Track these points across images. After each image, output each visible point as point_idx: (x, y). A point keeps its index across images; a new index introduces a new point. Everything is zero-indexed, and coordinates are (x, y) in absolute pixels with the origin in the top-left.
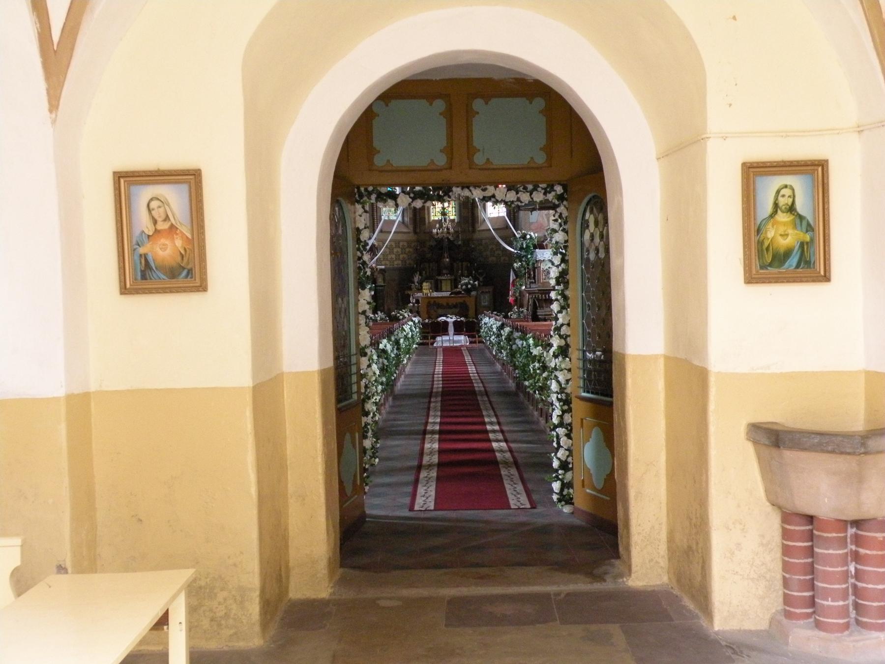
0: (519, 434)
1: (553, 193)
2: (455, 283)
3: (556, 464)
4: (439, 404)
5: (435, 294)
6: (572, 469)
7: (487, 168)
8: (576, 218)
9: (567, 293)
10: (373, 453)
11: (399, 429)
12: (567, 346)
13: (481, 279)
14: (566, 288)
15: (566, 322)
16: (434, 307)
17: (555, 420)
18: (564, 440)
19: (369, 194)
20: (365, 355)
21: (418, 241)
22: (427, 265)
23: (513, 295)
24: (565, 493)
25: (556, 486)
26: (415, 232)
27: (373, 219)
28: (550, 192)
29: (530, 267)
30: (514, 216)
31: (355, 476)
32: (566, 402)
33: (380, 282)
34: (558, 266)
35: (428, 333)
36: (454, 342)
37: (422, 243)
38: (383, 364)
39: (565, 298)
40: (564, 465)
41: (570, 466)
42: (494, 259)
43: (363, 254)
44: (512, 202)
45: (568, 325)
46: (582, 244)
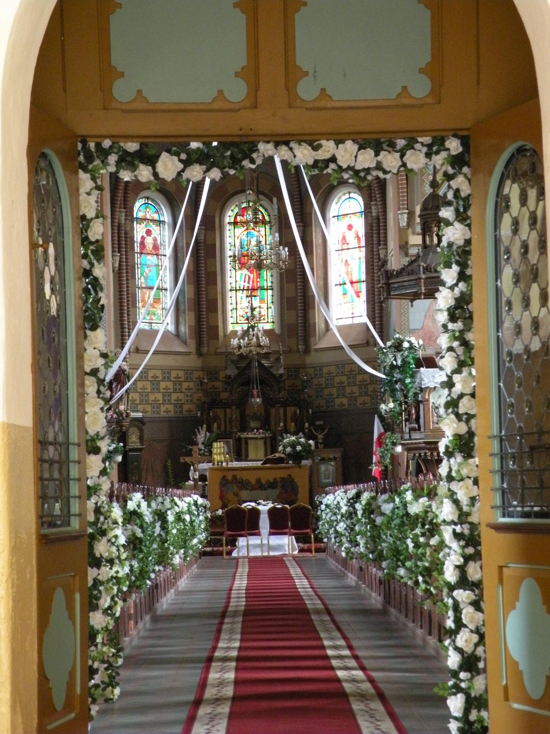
0: (386, 661)
1: (444, 154)
2: (272, 444)
3: (453, 660)
4: (239, 626)
5: (236, 464)
6: (485, 670)
7: (322, 105)
8: (486, 194)
9: (469, 336)
10: (110, 677)
11: (163, 656)
12: (471, 434)
13: (320, 437)
14: (468, 328)
15: (468, 391)
16: (230, 485)
17: (450, 575)
18: (468, 613)
19: (104, 153)
20: (96, 451)
21: (203, 369)
22: (220, 412)
23: (379, 463)
24: (473, 716)
25: (456, 704)
26: (200, 353)
27: (122, 328)
28: (437, 153)
29: (410, 400)
30: (381, 309)
31: (72, 674)
32: (471, 540)
33: (134, 440)
34: (452, 288)
35: (222, 534)
36: (271, 548)
37: (212, 373)
38: (134, 534)
39: (465, 344)
40: (470, 663)
41: (481, 665)
42: (345, 401)
43: (92, 265)
44: (368, 171)
45: (473, 395)
46: (497, 241)
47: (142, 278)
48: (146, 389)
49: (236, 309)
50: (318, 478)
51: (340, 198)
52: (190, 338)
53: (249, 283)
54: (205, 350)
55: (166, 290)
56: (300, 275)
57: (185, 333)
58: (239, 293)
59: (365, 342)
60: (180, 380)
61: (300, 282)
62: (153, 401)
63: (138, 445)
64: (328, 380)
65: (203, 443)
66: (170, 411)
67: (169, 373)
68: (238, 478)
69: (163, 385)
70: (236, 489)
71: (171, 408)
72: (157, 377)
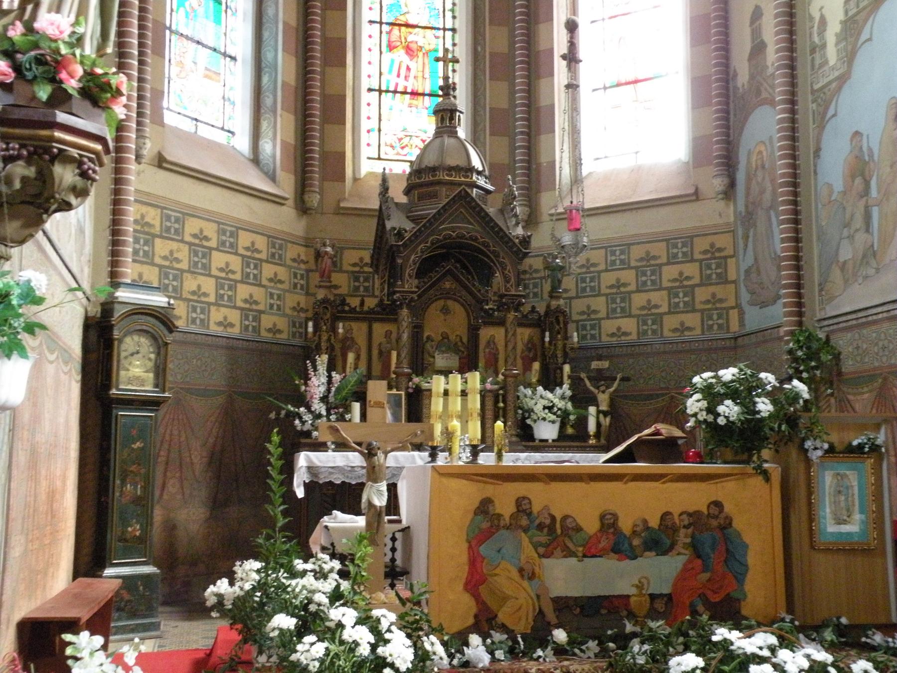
21: (308, 243)
22: (359, 330)
26: (303, 208)
37: (320, 260)
42: (629, 325)
48: (178, 260)
50: (811, 519)
54: (314, 199)
59: (692, 191)
60: (257, 256)
61: (522, 77)
64: (583, 280)
65: (324, 399)
66: (232, 325)
68: (536, 508)
69: (219, 260)
70: (528, 551)
71: (234, 316)
72: (206, 238)
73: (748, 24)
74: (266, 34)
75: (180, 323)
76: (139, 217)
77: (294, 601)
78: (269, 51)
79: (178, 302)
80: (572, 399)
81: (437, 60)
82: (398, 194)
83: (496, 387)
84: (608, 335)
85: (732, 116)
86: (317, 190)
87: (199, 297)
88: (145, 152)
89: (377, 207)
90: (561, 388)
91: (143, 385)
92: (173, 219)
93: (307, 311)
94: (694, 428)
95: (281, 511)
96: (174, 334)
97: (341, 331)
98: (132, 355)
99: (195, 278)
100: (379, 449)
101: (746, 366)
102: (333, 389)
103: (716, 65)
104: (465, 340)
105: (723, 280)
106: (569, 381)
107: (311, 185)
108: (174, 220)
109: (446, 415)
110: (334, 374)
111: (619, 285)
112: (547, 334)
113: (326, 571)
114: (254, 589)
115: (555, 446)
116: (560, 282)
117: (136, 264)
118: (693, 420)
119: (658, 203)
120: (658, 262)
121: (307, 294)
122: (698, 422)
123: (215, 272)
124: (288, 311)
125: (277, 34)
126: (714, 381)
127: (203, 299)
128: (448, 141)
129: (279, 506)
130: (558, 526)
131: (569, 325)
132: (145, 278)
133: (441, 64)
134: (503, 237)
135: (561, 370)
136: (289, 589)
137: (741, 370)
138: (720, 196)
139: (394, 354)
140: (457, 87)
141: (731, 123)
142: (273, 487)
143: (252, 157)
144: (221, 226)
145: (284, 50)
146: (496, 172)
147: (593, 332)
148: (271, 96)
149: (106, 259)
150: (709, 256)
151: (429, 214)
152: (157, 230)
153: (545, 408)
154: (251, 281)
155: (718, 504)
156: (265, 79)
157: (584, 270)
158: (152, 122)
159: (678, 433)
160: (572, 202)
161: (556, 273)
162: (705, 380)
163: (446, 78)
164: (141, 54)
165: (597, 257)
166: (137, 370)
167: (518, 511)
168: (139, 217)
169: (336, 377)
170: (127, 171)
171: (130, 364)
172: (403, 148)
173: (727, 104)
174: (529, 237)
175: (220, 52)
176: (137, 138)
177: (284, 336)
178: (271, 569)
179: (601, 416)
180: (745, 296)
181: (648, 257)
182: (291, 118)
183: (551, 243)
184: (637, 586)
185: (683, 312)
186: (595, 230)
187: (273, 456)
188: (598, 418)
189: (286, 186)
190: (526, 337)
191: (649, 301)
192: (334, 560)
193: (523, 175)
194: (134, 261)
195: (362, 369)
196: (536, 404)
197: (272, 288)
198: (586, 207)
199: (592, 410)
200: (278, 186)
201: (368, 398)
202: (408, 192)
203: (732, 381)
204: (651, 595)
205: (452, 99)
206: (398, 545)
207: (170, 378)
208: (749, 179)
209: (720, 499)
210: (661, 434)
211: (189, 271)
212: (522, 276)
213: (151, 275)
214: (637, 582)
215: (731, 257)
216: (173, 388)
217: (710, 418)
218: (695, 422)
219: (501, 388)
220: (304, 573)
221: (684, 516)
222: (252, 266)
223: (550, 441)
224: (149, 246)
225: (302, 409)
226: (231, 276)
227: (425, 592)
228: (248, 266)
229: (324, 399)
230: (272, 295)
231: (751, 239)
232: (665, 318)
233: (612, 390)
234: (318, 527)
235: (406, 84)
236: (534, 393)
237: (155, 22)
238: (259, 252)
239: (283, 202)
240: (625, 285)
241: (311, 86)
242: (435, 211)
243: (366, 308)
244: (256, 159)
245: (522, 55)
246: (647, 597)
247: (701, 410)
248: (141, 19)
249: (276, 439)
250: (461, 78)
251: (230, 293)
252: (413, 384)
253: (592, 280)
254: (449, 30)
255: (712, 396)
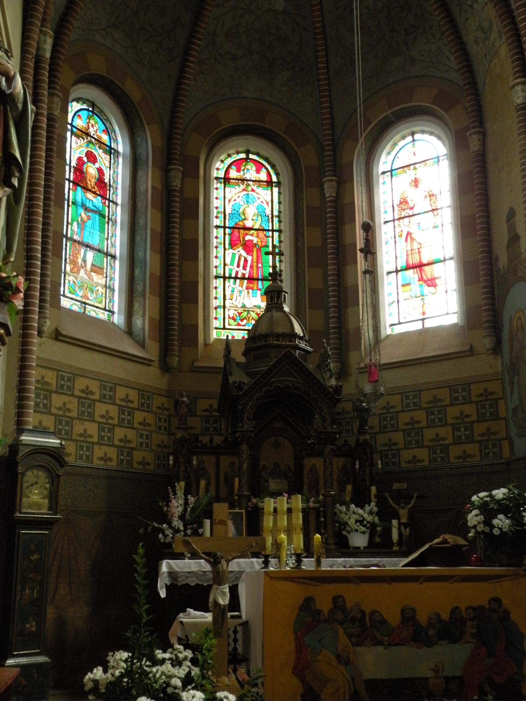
21: (169, 394)
22: (209, 461)
26: (165, 367)
37: (178, 408)
42: (423, 454)
47: (75, 224)
48: (69, 410)
49: (224, 307)
51: (395, 144)
52: (150, 338)
53: (244, 268)
54: (174, 361)
55: (114, 257)
56: (332, 254)
57: (143, 329)
58: (230, 283)
59: (467, 348)
60: (130, 405)
62: (81, 435)
63: (43, 512)
64: (385, 419)
65: (182, 517)
66: (110, 460)
67: (113, 389)
68: (349, 605)
69: (101, 409)
70: (343, 640)
71: (112, 453)
72: (91, 393)
73: (505, 221)
74: (138, 238)
75: (70, 460)
76: (40, 378)
77: (154, 685)
78: (140, 251)
79: (68, 442)
80: (378, 514)
81: (267, 253)
82: (238, 355)
83: (317, 505)
84: (406, 462)
85: (496, 291)
86: (177, 354)
87: (85, 438)
88: (45, 329)
89: (222, 365)
90: (369, 505)
91: (40, 509)
92: (66, 379)
93: (169, 447)
94: (474, 538)
95: (146, 610)
96: (65, 468)
97: (195, 462)
98: (32, 485)
99: (83, 423)
100: (222, 558)
101: (514, 487)
102: (189, 509)
103: (482, 252)
104: (292, 468)
105: (495, 417)
106: (376, 500)
107: (173, 350)
108: (66, 379)
109: (275, 530)
110: (189, 497)
111: (413, 422)
112: (357, 462)
113: (181, 659)
114: (122, 675)
115: (366, 553)
116: (366, 421)
117: (37, 414)
118: (473, 531)
119: (437, 359)
120: (444, 403)
121: (170, 434)
122: (477, 532)
123: (98, 418)
124: (154, 448)
125: (146, 237)
126: (488, 499)
127: (89, 440)
128: (276, 314)
129: (144, 606)
130: (367, 618)
131: (374, 455)
132: (44, 424)
133: (271, 256)
134: (321, 388)
135: (370, 491)
136: (151, 675)
137: (510, 490)
138: (490, 352)
139: (237, 480)
140: (283, 273)
141: (496, 295)
142: (139, 590)
143: (127, 330)
144: (103, 383)
145: (151, 249)
146: (313, 337)
147: (394, 460)
148: (142, 285)
149: (13, 411)
150: (483, 398)
151: (262, 370)
152: (54, 388)
153: (357, 521)
154: (126, 425)
155: (497, 600)
156: (137, 272)
157: (385, 411)
158: (51, 306)
159: (461, 541)
160: (371, 360)
161: (363, 414)
162: (482, 499)
163: (274, 267)
164: (44, 256)
165: (395, 400)
166: (36, 497)
167: (335, 607)
168: (40, 378)
169: (191, 499)
170: (32, 344)
171: (31, 492)
172: (242, 320)
173: (492, 281)
174: (341, 387)
175: (103, 252)
176: (39, 318)
177: (151, 467)
178: (136, 658)
179: (402, 528)
180: (513, 430)
181: (436, 400)
182: (157, 300)
183: (355, 392)
184: (434, 670)
185: (465, 443)
186: (390, 380)
187: (139, 565)
188: (399, 529)
189: (152, 352)
190: (341, 464)
191: (437, 434)
192: (187, 650)
193: (336, 338)
194: (35, 411)
195: (212, 492)
196: (350, 518)
197: (142, 430)
198: (382, 362)
199: (395, 522)
200: (147, 352)
201: (214, 517)
202: (245, 353)
203: (504, 499)
204: (445, 677)
205: (279, 282)
206: (239, 636)
207: (61, 502)
208: (511, 340)
209: (498, 596)
210: (448, 543)
211: (78, 418)
212: (336, 417)
213: (49, 422)
214: (434, 667)
215: (501, 399)
216: (64, 510)
217: (487, 530)
218: (475, 533)
219: (321, 506)
220: (163, 662)
221: (470, 611)
222: (126, 413)
223: (362, 548)
224: (47, 400)
225: (164, 526)
226: (110, 421)
227: (260, 677)
228: (123, 413)
229: (182, 517)
230: (141, 435)
231: (516, 384)
232: (451, 448)
233: (409, 506)
234: (176, 623)
235: (244, 272)
236: (348, 509)
237: (55, 232)
238: (132, 402)
239: (150, 363)
240: (418, 422)
241: (172, 276)
242: (266, 368)
243: (214, 444)
244: (129, 330)
245: (332, 248)
246: (443, 679)
247: (479, 523)
248: (44, 230)
249: (141, 551)
250: (285, 267)
251: (109, 435)
252: (252, 504)
253: (392, 418)
254: (276, 231)
255: (488, 511)
